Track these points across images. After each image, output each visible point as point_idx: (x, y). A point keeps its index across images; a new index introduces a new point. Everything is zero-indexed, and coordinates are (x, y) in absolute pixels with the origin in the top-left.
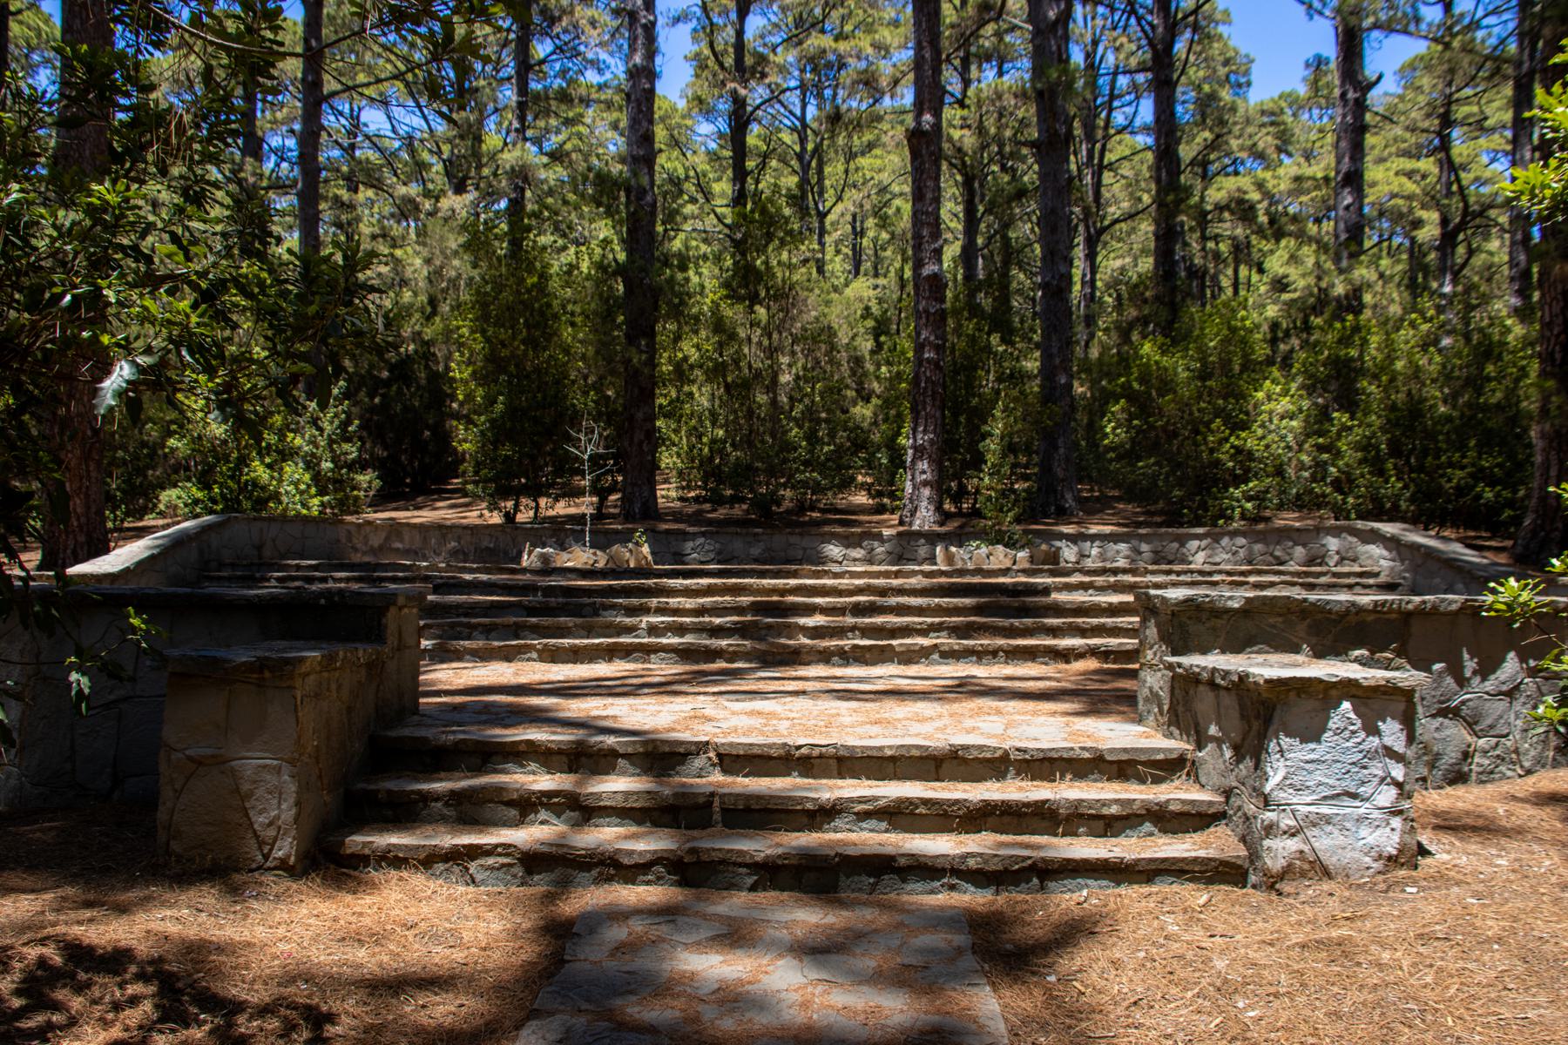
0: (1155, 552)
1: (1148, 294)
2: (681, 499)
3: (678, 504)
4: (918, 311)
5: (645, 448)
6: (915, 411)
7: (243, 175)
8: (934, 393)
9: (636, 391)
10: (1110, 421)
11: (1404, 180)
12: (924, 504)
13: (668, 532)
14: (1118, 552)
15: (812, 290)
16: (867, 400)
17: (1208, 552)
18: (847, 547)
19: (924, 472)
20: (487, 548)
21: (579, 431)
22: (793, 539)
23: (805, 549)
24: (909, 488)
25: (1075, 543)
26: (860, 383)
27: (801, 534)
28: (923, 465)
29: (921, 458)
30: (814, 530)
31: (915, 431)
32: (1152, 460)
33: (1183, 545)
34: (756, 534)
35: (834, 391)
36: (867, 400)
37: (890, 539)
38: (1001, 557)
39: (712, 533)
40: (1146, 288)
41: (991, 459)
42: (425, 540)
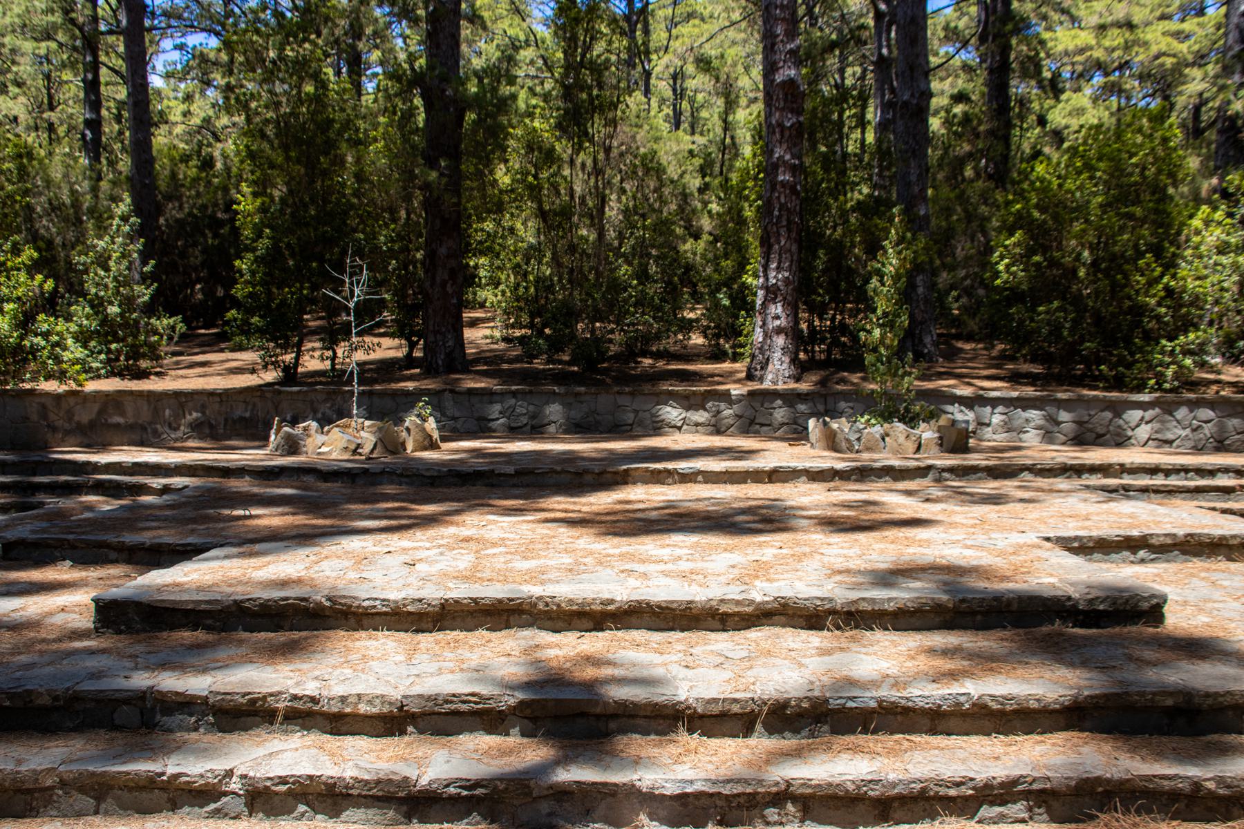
0: (1079, 423)
1: (982, 128)
2: (506, 339)
3: (502, 346)
4: (769, 125)
5: (449, 290)
6: (766, 243)
7: (74, 15)
8: (789, 222)
9: (438, 222)
10: (1002, 257)
11: (1169, 39)
12: (778, 355)
13: (471, 392)
14: (1027, 420)
15: (641, 127)
16: (697, 237)
17: (1156, 425)
18: (688, 409)
19: (777, 317)
20: (242, 419)
21: (343, 272)
22: (622, 400)
23: (636, 412)
24: (758, 336)
25: (971, 408)
26: (689, 221)
27: (632, 394)
28: (777, 309)
29: (774, 301)
30: (647, 388)
31: (766, 268)
32: (1056, 304)
33: (1118, 415)
34: (578, 394)
35: (662, 227)
36: (697, 237)
37: (741, 399)
38: (902, 439)
39: (523, 393)
40: (980, 123)
41: (881, 306)
42: (156, 412)
